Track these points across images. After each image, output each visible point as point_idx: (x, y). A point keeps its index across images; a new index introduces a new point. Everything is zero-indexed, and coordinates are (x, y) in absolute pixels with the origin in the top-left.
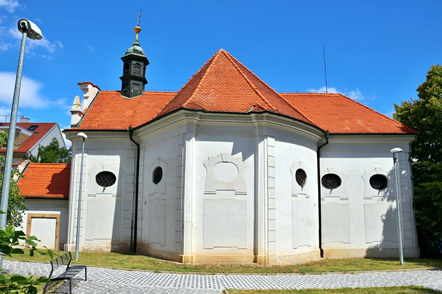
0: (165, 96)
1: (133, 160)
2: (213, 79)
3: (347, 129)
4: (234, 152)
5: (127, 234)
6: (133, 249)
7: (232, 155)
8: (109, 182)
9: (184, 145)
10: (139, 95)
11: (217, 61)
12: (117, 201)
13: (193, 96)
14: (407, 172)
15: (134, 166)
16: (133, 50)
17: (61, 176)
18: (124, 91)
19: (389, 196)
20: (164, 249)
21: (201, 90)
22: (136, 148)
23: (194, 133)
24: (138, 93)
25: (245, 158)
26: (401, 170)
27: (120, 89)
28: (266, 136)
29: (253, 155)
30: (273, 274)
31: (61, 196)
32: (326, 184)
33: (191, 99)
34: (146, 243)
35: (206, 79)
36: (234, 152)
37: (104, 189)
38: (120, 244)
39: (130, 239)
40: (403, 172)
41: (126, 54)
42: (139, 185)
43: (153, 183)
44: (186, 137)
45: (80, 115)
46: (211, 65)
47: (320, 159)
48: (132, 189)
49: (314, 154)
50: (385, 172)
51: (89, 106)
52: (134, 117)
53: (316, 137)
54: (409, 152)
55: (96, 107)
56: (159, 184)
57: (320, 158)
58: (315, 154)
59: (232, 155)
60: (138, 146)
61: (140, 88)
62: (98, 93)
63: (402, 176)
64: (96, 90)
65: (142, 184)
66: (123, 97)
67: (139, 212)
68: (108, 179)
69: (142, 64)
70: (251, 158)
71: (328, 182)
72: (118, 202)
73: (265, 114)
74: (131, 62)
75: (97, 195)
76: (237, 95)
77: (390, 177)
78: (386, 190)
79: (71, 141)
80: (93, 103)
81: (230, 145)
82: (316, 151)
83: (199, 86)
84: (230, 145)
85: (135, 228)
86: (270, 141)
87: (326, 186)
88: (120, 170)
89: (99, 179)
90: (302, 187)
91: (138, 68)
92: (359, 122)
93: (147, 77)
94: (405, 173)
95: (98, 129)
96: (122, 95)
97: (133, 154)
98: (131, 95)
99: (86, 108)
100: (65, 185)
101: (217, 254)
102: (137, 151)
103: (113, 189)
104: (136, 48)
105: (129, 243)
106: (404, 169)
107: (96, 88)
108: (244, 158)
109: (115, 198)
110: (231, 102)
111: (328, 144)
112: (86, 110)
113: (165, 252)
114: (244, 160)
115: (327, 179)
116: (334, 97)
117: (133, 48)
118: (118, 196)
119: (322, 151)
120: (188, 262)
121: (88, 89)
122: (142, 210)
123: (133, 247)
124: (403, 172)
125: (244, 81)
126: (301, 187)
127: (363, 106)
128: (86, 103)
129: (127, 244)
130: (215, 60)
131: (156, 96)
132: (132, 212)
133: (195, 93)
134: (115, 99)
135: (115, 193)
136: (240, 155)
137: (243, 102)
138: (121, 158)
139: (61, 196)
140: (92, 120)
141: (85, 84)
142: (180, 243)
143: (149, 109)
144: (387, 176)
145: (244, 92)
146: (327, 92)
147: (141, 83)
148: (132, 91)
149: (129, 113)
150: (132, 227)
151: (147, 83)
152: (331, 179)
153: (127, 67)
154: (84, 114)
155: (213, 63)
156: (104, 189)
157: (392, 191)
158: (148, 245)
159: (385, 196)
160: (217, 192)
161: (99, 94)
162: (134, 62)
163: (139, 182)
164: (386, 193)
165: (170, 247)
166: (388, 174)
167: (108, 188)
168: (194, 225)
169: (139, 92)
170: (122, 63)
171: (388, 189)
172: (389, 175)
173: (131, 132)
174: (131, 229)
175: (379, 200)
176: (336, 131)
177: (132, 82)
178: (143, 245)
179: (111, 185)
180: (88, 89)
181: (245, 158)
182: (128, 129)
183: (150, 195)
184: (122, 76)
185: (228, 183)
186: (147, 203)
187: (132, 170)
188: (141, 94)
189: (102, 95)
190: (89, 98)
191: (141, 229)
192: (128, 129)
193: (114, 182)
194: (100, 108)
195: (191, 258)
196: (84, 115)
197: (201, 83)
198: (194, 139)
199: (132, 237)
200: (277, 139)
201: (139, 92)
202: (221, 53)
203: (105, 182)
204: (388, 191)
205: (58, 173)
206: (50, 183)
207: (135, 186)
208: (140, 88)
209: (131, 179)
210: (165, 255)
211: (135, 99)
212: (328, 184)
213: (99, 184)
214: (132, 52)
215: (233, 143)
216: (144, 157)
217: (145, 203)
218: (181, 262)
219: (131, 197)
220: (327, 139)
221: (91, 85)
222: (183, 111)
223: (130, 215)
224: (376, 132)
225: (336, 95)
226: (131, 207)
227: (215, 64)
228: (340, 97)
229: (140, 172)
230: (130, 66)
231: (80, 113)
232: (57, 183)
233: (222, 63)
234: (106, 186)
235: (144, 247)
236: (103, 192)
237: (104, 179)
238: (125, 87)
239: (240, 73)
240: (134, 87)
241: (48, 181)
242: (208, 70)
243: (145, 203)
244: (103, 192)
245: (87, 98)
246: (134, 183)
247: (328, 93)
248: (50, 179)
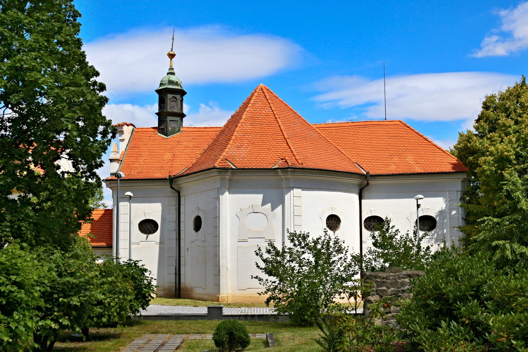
0: (205, 132)
1: (174, 207)
3: (393, 169)
4: (264, 203)
5: (171, 279)
6: (177, 294)
7: (262, 206)
8: (152, 229)
9: (218, 199)
10: (177, 132)
11: (256, 101)
12: (160, 248)
13: (227, 150)
14: (458, 212)
15: (175, 213)
16: (167, 82)
17: (100, 223)
18: (162, 129)
19: (436, 238)
21: (235, 141)
22: (177, 195)
23: (227, 187)
24: (176, 131)
25: (273, 208)
26: (451, 210)
27: (157, 126)
28: (293, 188)
29: (281, 206)
31: (104, 244)
32: (369, 226)
33: (224, 154)
34: (189, 288)
35: (241, 127)
36: (264, 203)
37: (147, 237)
38: (165, 290)
39: (174, 284)
40: (454, 212)
41: (160, 86)
42: (181, 232)
44: (220, 191)
45: (118, 163)
46: (248, 109)
47: (362, 201)
48: (174, 235)
49: (355, 197)
50: (433, 214)
51: (126, 150)
52: (173, 162)
54: (461, 191)
55: (133, 150)
56: (199, 232)
57: (362, 200)
58: (357, 197)
59: (262, 206)
60: (179, 193)
61: (178, 125)
62: (133, 131)
63: (451, 218)
64: (131, 127)
65: (184, 223)
66: (160, 136)
67: (182, 259)
68: (151, 226)
69: (178, 97)
70: (279, 208)
71: (372, 224)
72: (161, 249)
73: (289, 170)
74: (166, 96)
75: (140, 243)
76: (269, 147)
77: (438, 218)
78: (433, 232)
79: (112, 189)
80: (129, 145)
81: (259, 197)
82: (358, 194)
83: (233, 137)
84: (260, 197)
86: (297, 192)
87: (368, 228)
88: (162, 218)
89: (142, 227)
90: (334, 232)
91: (175, 101)
92: (410, 159)
93: (185, 111)
94: (455, 214)
95: (138, 177)
96: (159, 132)
97: (174, 201)
98: (168, 133)
99: (123, 152)
100: (106, 232)
101: (250, 294)
102: (178, 198)
103: (156, 236)
104: (171, 79)
105: (173, 289)
106: (454, 209)
107: (130, 126)
108: (273, 208)
109: (158, 245)
110: (261, 155)
111: (369, 186)
113: (205, 295)
114: (272, 210)
115: (370, 221)
116: (393, 125)
117: (168, 79)
118: (161, 243)
119: (365, 193)
120: (224, 301)
121: (123, 131)
122: (185, 257)
123: (177, 292)
124: (454, 212)
125: (278, 128)
126: (333, 232)
127: (422, 136)
128: (123, 146)
129: (171, 290)
130: (252, 102)
131: (195, 133)
132: (175, 258)
133: (229, 146)
134: (152, 139)
135: (158, 240)
136: (269, 206)
137: (272, 155)
138: (162, 206)
139: (104, 244)
140: (130, 166)
141: (120, 127)
142: (218, 285)
143: (188, 150)
144: (435, 217)
145: (276, 143)
146: (386, 119)
147: (178, 119)
148: (170, 128)
149: (168, 156)
150: (176, 273)
152: (374, 221)
153: (162, 102)
154: (121, 159)
155: (250, 105)
156: (147, 237)
157: (440, 233)
158: (192, 289)
159: (432, 239)
160: (249, 240)
161: (134, 133)
162: (170, 96)
163: (181, 229)
164: (433, 235)
165: (210, 290)
166: (436, 215)
167: (151, 236)
168: (229, 269)
169: (177, 129)
171: (436, 231)
172: (437, 216)
173: (172, 180)
174: (175, 275)
175: (426, 242)
177: (169, 118)
178: (187, 290)
179: (154, 232)
180: (123, 131)
181: (273, 208)
182: (168, 178)
183: (192, 242)
184: (157, 112)
185: (259, 231)
186: (189, 249)
187: (174, 217)
188: (179, 131)
189: (137, 133)
190: (125, 141)
191: (185, 274)
192: (168, 178)
193: (157, 229)
194: (137, 150)
195: (226, 297)
196: (121, 161)
197: (235, 133)
198: (227, 193)
199: (176, 283)
200: (304, 189)
201: (177, 129)
202: (261, 90)
203: (148, 229)
204: (435, 232)
205: (97, 219)
206: (90, 231)
207: (178, 232)
208: (178, 125)
209: (173, 226)
210: (206, 297)
211: (174, 138)
212: (371, 227)
213: (142, 232)
214: (167, 84)
216: (184, 204)
217: (188, 250)
218: (218, 301)
219: (174, 243)
220: (367, 181)
221: (125, 125)
222: (216, 170)
224: (422, 171)
225: (396, 123)
226: (175, 253)
227: (252, 106)
228: (399, 125)
229: (182, 220)
230: (166, 100)
232: (97, 230)
234: (148, 234)
235: (188, 291)
236: (146, 240)
237: (146, 227)
238: (162, 125)
239: (276, 119)
241: (87, 229)
243: (188, 250)
244: (146, 240)
245: (122, 140)
246: (176, 230)
247: (387, 120)
248: (90, 227)
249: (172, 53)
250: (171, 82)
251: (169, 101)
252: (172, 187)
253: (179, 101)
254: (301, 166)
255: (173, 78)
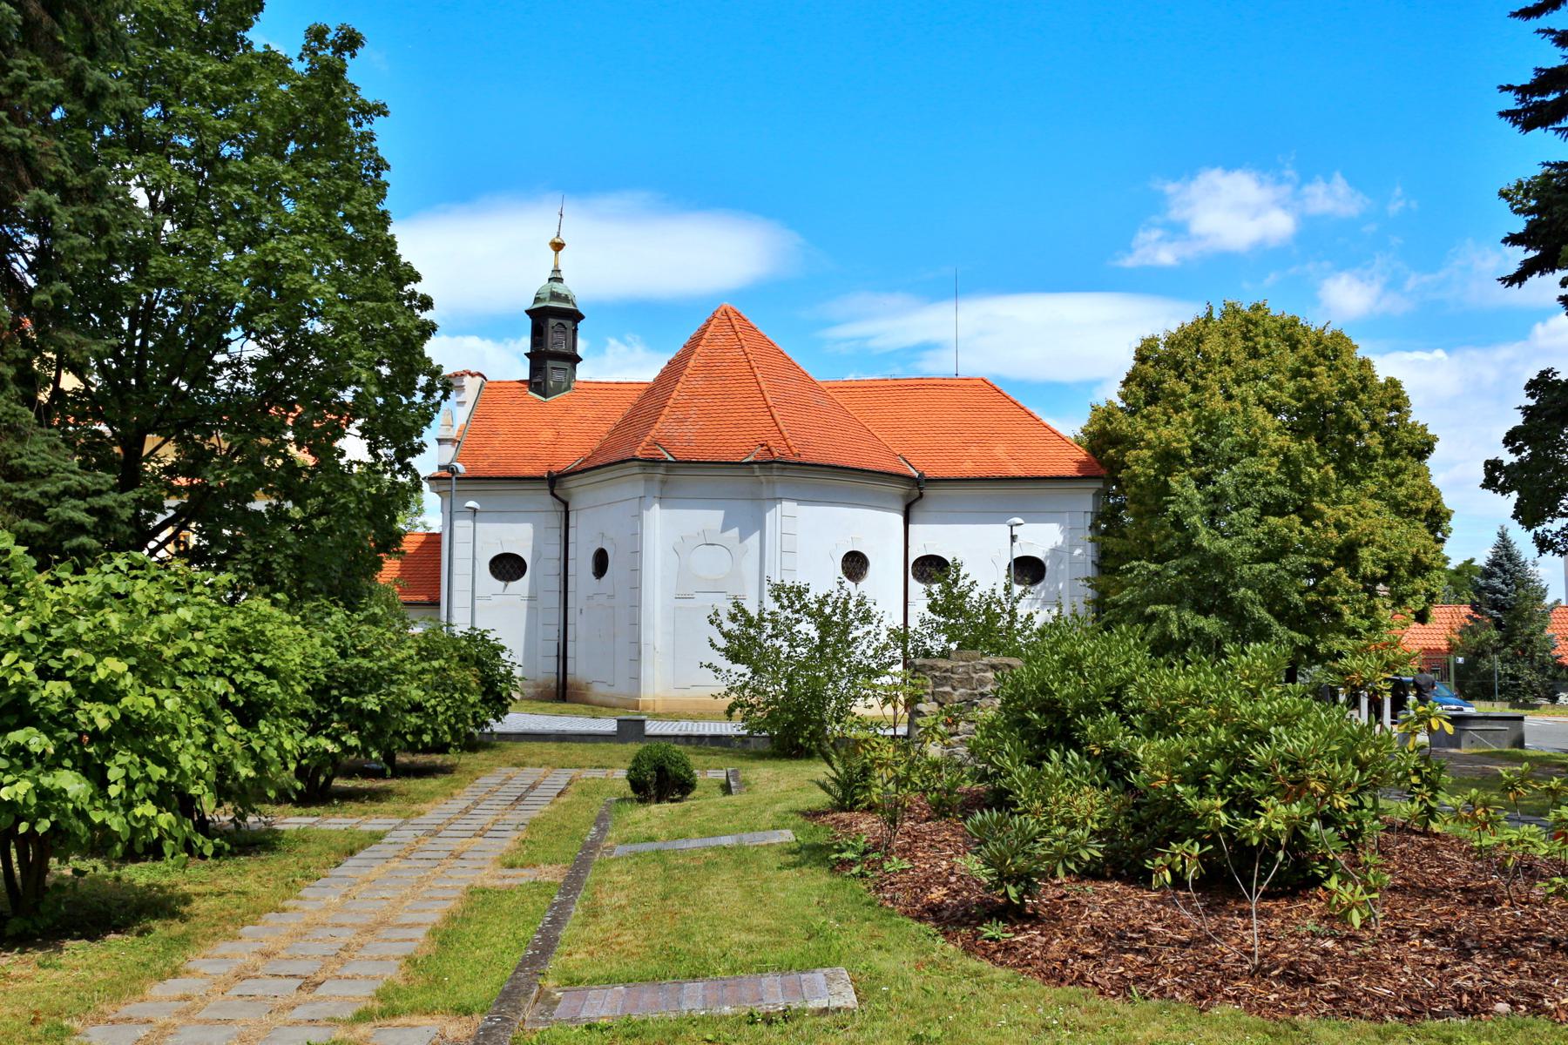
2: (698, 384)
4: (726, 527)
9: (639, 516)
12: (529, 608)
13: (657, 426)
14: (1085, 551)
20: (613, 690)
26: (1073, 546)
27: (526, 377)
30: (734, 695)
31: (423, 598)
33: (652, 432)
36: (726, 527)
40: (1078, 552)
43: (594, 578)
46: (699, 350)
47: (911, 526)
53: (900, 489)
58: (900, 519)
60: (566, 505)
64: (479, 379)
67: (570, 629)
68: (512, 567)
69: (568, 323)
74: (545, 321)
78: (1039, 587)
83: (670, 402)
85: (563, 657)
86: (788, 507)
92: (1000, 451)
93: (580, 352)
95: (490, 474)
97: (555, 520)
98: (548, 391)
103: (521, 586)
105: (554, 684)
108: (742, 539)
112: (462, 430)
119: (915, 513)
121: (393, 236)
124: (1078, 552)
133: (662, 418)
135: (526, 593)
136: (735, 532)
142: (636, 678)
147: (566, 365)
149: (547, 435)
151: (582, 317)
152: (931, 565)
153: (538, 333)
155: (703, 342)
160: (696, 595)
162: (552, 322)
169: (564, 385)
170: (528, 321)
172: (1047, 558)
173: (553, 482)
176: (940, 474)
177: (550, 364)
180: (393, 236)
187: (555, 550)
188: (568, 388)
197: (674, 395)
201: (564, 385)
209: (555, 566)
215: (721, 513)
220: (920, 489)
223: (554, 633)
224: (1023, 474)
225: (976, 383)
226: (555, 617)
231: (453, 441)
233: (719, 342)
240: (554, 377)
242: (692, 363)
245: (461, 403)
249: (558, 240)
250: (555, 296)
251: (550, 331)
252: (553, 494)
253: (570, 332)
254: (797, 459)
255: (558, 288)
